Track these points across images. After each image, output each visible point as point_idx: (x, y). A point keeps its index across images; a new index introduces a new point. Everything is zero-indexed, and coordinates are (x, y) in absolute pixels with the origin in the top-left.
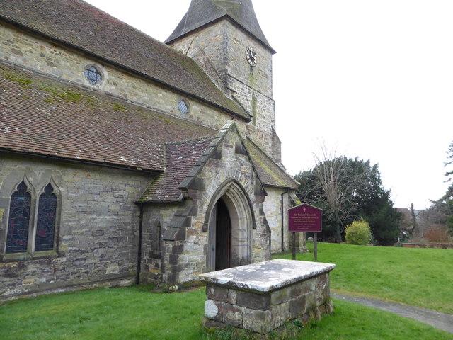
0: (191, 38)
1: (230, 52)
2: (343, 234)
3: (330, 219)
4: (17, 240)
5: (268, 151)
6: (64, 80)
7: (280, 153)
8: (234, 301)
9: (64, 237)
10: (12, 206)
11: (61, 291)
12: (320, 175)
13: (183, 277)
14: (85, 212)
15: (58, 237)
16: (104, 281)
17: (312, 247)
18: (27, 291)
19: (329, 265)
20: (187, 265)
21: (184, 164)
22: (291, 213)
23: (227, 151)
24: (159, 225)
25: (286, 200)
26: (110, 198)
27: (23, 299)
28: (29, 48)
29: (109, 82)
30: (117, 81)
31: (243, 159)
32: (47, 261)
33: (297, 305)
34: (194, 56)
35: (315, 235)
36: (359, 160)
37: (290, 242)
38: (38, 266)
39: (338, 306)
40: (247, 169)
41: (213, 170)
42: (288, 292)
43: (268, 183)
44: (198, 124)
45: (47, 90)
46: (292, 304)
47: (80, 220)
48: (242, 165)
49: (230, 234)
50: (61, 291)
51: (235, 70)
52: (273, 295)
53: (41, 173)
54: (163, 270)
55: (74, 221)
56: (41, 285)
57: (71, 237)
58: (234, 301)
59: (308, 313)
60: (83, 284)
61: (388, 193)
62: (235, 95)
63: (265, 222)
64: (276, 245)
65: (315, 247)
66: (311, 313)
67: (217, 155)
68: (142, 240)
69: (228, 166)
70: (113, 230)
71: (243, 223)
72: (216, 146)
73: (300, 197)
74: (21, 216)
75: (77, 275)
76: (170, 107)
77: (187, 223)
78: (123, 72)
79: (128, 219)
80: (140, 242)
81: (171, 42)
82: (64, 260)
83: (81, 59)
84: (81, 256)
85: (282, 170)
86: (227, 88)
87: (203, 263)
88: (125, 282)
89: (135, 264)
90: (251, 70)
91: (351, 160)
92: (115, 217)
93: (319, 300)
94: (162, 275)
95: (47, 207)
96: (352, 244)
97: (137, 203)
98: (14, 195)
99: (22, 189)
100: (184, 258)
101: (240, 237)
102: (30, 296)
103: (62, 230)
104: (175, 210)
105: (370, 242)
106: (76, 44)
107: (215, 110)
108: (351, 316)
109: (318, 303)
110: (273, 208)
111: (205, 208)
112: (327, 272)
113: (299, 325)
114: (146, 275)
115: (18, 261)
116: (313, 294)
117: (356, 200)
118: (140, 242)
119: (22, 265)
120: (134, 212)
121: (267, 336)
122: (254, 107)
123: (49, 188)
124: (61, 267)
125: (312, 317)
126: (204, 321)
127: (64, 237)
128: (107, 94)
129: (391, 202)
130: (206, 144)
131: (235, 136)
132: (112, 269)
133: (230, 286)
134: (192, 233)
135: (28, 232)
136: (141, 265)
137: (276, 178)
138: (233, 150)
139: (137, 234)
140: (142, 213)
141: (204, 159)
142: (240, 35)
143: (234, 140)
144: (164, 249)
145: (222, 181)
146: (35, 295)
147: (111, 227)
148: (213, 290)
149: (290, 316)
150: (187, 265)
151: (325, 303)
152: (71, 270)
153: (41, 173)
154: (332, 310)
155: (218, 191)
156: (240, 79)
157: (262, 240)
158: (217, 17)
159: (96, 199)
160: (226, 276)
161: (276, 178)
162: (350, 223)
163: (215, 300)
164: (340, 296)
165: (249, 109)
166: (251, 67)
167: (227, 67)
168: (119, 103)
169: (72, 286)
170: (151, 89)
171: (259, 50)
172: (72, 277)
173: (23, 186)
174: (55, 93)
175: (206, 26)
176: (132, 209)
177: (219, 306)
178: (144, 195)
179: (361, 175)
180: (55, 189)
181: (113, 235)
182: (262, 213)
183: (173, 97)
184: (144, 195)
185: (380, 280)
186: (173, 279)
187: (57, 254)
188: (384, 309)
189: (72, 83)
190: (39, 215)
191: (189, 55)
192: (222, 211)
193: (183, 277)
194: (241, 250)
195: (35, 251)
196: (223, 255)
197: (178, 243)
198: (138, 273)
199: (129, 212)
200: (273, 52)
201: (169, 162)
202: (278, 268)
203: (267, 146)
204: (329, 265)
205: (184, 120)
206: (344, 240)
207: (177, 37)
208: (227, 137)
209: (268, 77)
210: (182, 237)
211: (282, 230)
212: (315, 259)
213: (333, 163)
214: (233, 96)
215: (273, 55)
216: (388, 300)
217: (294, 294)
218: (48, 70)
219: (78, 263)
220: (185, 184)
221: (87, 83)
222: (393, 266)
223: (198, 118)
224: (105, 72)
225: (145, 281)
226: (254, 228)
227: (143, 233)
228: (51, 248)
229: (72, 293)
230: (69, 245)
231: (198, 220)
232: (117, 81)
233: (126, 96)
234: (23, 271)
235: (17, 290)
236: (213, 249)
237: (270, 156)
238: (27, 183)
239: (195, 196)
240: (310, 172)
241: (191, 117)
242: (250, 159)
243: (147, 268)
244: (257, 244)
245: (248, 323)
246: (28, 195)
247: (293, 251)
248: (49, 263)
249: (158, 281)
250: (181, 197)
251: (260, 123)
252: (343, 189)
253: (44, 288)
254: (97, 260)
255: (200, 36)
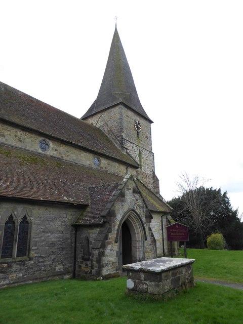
0: (99, 115)
1: (125, 124)
2: (206, 242)
3: (196, 230)
4: (7, 252)
5: (150, 187)
6: (28, 150)
7: (159, 187)
8: (142, 279)
9: (33, 248)
10: (5, 229)
11: (31, 282)
12: (186, 201)
13: (106, 271)
14: (44, 232)
15: (29, 248)
16: (55, 276)
17: (183, 252)
18: (12, 282)
19: (192, 260)
20: (107, 264)
21: (102, 200)
22: (168, 229)
23: (128, 192)
24: (87, 239)
25: (164, 220)
26: (58, 223)
27: (10, 287)
28: (9, 133)
29: (53, 150)
30: (58, 148)
31: (137, 196)
32: (22, 263)
33: (176, 281)
34: (101, 126)
35: (185, 244)
36: (213, 189)
37: (168, 249)
38: (18, 266)
39: (198, 283)
40: (140, 202)
41: (120, 205)
42: (170, 273)
43: (153, 209)
44: (106, 172)
45: (19, 157)
46: (172, 280)
47: (41, 237)
48: (137, 200)
49: (131, 244)
50: (31, 282)
51: (128, 135)
52: (163, 275)
53: (22, 209)
54: (92, 267)
55: (38, 237)
56: (20, 278)
57: (36, 248)
58: (142, 279)
59: (181, 286)
60: (43, 278)
61: (236, 212)
62: (128, 151)
63: (152, 235)
64: (159, 251)
65: (185, 251)
66: (183, 286)
67: (122, 195)
68: (77, 249)
69: (129, 201)
70: (59, 243)
71: (139, 237)
72: (122, 190)
73: (174, 217)
74: (9, 235)
75: (40, 272)
76: (88, 163)
77: (106, 238)
78: (61, 143)
79: (68, 236)
80: (75, 250)
81: (85, 118)
82: (32, 262)
83: (37, 137)
84: (42, 260)
85: (160, 199)
86: (123, 147)
87: (116, 263)
88: (67, 277)
89: (72, 265)
90: (138, 134)
91: (207, 189)
92: (61, 235)
93: (187, 279)
94: (91, 271)
95: (23, 230)
96: (213, 249)
97: (73, 225)
98: (7, 223)
99: (11, 219)
100: (105, 259)
101: (137, 245)
102: (14, 285)
103: (32, 243)
104: (98, 229)
105: (225, 248)
106: (35, 128)
107: (116, 162)
108: (205, 288)
109: (187, 281)
110: (156, 225)
111: (116, 228)
112: (191, 263)
113: (177, 292)
114: (80, 271)
115: (7, 263)
116: (184, 275)
117: (213, 217)
118: (75, 250)
119: (10, 266)
120: (72, 231)
121: (161, 296)
122: (140, 158)
123: (25, 218)
124: (31, 266)
125: (184, 288)
126: (127, 291)
127: (33, 248)
128: (51, 156)
129: (238, 219)
130: (115, 188)
131: (132, 182)
132: (59, 268)
133: (141, 270)
134: (109, 243)
135: (13, 245)
136: (76, 266)
137: (158, 206)
138: (131, 191)
139: (73, 245)
140: (76, 231)
141: (115, 198)
142: (130, 113)
143: (132, 185)
144: (93, 255)
145: (125, 211)
146: (16, 284)
147: (59, 241)
148: (131, 274)
149: (172, 287)
150: (107, 264)
151: (191, 281)
152: (36, 269)
153: (22, 209)
154: (195, 285)
155: (123, 217)
156: (131, 141)
157: (151, 247)
158: (115, 103)
159: (50, 223)
160: (137, 266)
161: (158, 206)
162: (209, 234)
163: (132, 279)
164: (199, 279)
165: (137, 160)
166: (138, 132)
167: (123, 134)
168: (59, 162)
169: (37, 279)
170: (77, 152)
171: (143, 122)
172: (37, 273)
173: (11, 217)
174: (24, 158)
175: (109, 108)
176: (70, 229)
177: (135, 282)
178: (78, 221)
179: (215, 200)
180: (28, 218)
181: (60, 246)
182: (150, 229)
183: (90, 156)
184: (78, 221)
185: (225, 271)
186: (99, 273)
187: (28, 259)
188: (226, 286)
189: (32, 151)
190: (19, 234)
191: (98, 126)
192: (126, 228)
193: (106, 271)
194: (139, 255)
195: (17, 256)
196: (127, 255)
197: (101, 250)
198: (75, 270)
199: (69, 231)
200: (151, 122)
201: (92, 199)
202: (164, 262)
203: (149, 183)
204: (192, 260)
205: (97, 170)
206: (207, 247)
207: (90, 114)
208: (128, 184)
209: (148, 138)
210: (104, 246)
211: (163, 240)
212: (186, 257)
213: (195, 192)
214: (127, 152)
215: (152, 124)
216: (229, 281)
217: (173, 274)
218: (19, 145)
219: (40, 264)
220: (104, 213)
221: (40, 151)
222: (236, 262)
223: (106, 168)
224: (51, 144)
225: (79, 275)
226: (146, 240)
227: (77, 244)
228: (25, 255)
229: (36, 283)
230: (35, 253)
231: (112, 236)
232: (58, 148)
233: (62, 157)
234: (10, 269)
235: (7, 282)
236: (121, 254)
237: (152, 190)
238: (13, 215)
239: (110, 221)
240: (179, 198)
241: (102, 168)
242: (141, 196)
243: (80, 267)
244: (148, 250)
245: (151, 290)
246: (14, 222)
247: (171, 254)
248: (24, 265)
249: (88, 275)
250: (102, 221)
251: (145, 168)
252: (203, 210)
253: (21, 280)
254: (50, 262)
255: (105, 115)
